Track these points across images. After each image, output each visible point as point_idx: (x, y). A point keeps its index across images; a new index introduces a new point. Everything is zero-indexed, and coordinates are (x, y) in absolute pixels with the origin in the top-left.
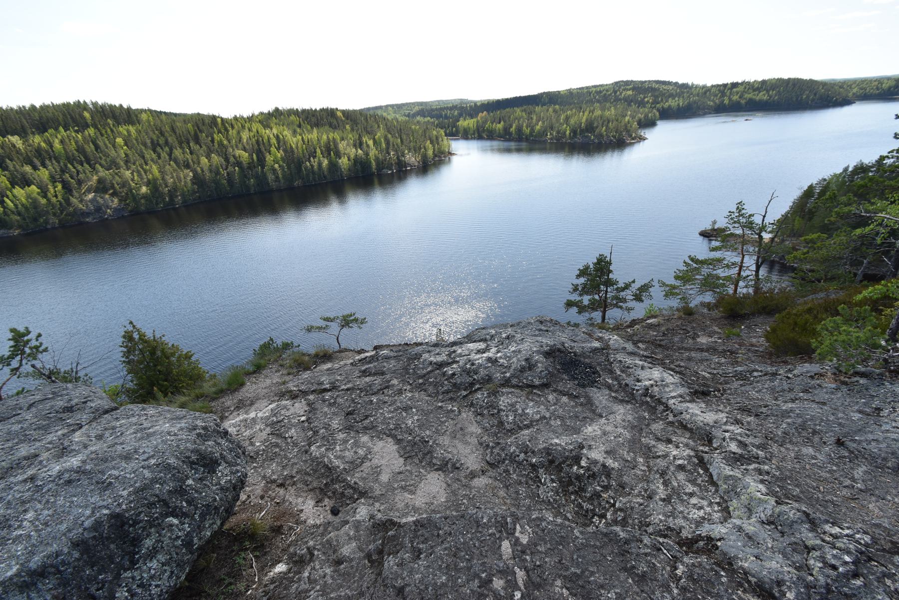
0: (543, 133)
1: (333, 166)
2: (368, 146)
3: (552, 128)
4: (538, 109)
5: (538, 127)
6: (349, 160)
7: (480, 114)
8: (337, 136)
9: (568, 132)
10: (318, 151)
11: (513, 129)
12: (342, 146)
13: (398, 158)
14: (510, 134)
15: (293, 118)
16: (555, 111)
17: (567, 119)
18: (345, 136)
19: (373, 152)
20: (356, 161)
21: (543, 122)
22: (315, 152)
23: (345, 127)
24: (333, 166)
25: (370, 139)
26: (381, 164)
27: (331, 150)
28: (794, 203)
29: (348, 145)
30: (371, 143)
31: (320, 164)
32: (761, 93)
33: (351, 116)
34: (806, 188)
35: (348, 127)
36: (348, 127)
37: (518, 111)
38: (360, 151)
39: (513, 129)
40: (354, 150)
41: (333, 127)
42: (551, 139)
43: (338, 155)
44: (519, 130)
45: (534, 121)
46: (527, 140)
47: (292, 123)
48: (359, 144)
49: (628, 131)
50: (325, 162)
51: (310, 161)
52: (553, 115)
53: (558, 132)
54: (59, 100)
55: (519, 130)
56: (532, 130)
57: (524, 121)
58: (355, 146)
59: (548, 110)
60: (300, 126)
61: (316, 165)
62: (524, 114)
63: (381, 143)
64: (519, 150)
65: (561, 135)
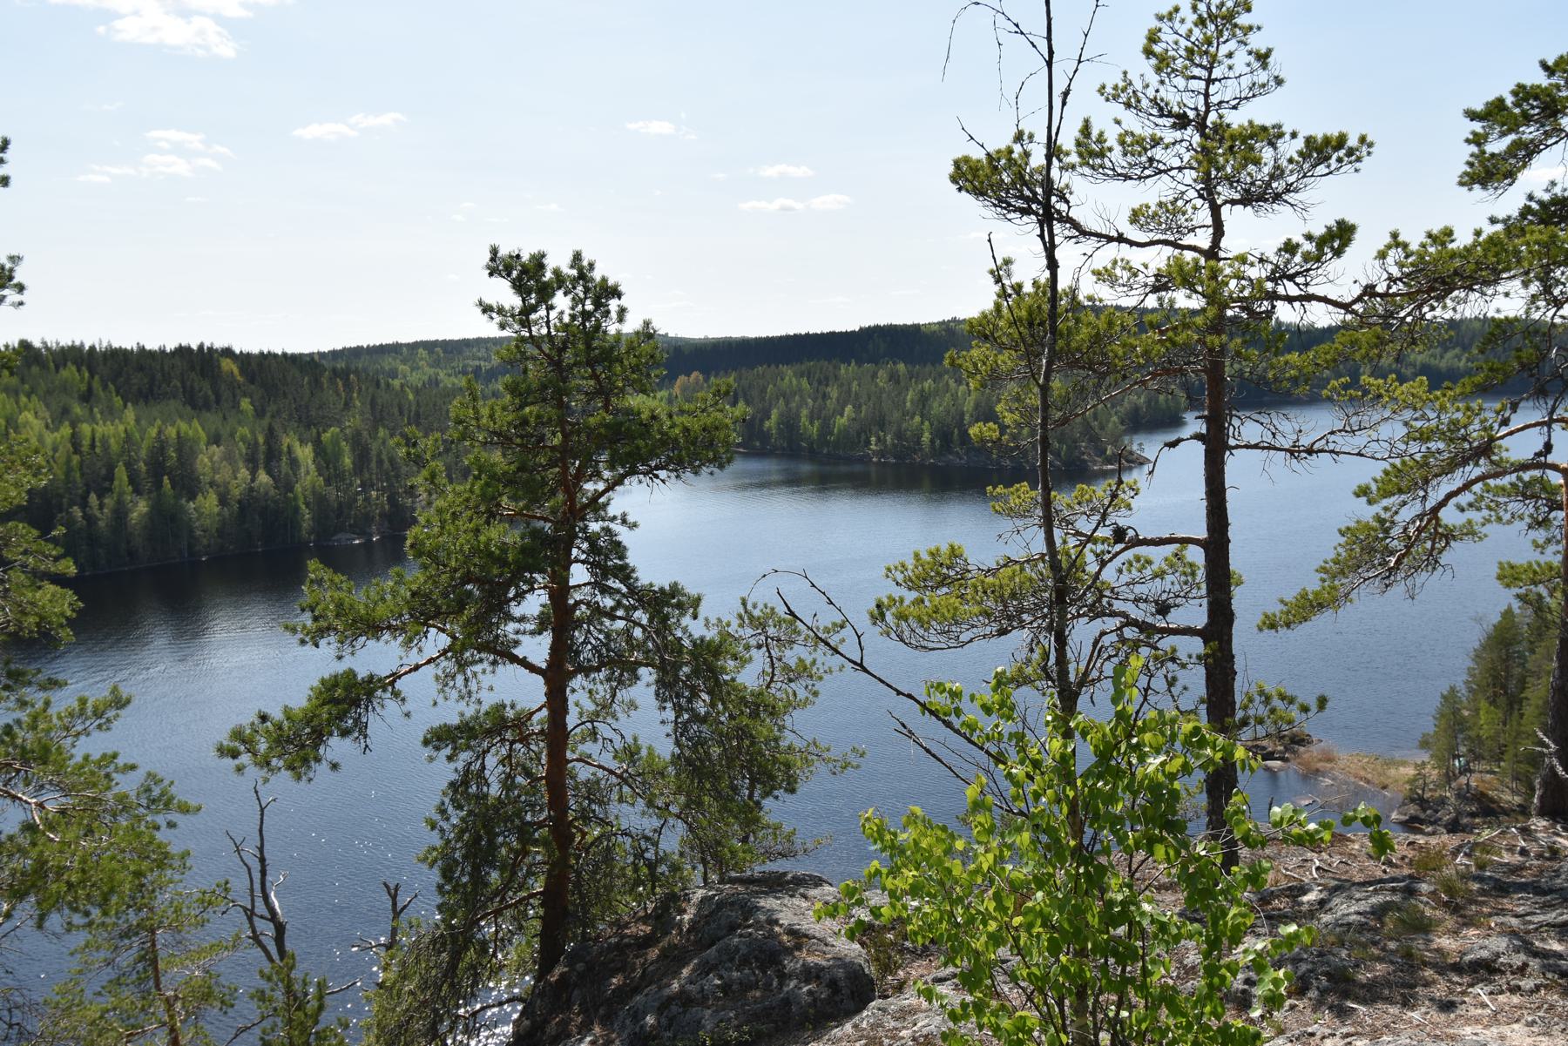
0: (859, 435)
1: (166, 520)
2: (294, 463)
3: (882, 423)
4: (846, 370)
5: (841, 421)
6: (223, 501)
7: (682, 379)
8: (194, 429)
9: (926, 437)
10: (121, 473)
11: (771, 423)
12: (207, 460)
13: (392, 500)
14: (765, 437)
15: (69, 372)
16: (894, 378)
17: (924, 399)
18: (225, 432)
19: (309, 476)
20: (249, 505)
21: (857, 408)
22: (110, 477)
23: (236, 406)
24: (166, 520)
25: (302, 442)
26: (332, 517)
27: (170, 472)
28: (1478, 657)
29: (228, 457)
30: (305, 453)
31: (120, 513)
32: (1449, 355)
33: (268, 372)
34: (1495, 618)
35: (245, 404)
36: (245, 404)
37: (789, 376)
38: (263, 477)
39: (771, 423)
40: (244, 473)
41: (196, 404)
42: (881, 454)
43: (189, 486)
44: (790, 424)
45: (831, 404)
46: (813, 454)
47: (65, 388)
48: (269, 455)
49: (1094, 439)
50: (140, 508)
51: (84, 504)
52: (888, 387)
53: (899, 435)
54: (901, 322)
55: (790, 424)
56: (826, 429)
57: (803, 402)
58: (252, 462)
59: (874, 376)
60: (87, 397)
61: (104, 518)
62: (804, 382)
63: (338, 455)
64: (792, 482)
65: (906, 447)
